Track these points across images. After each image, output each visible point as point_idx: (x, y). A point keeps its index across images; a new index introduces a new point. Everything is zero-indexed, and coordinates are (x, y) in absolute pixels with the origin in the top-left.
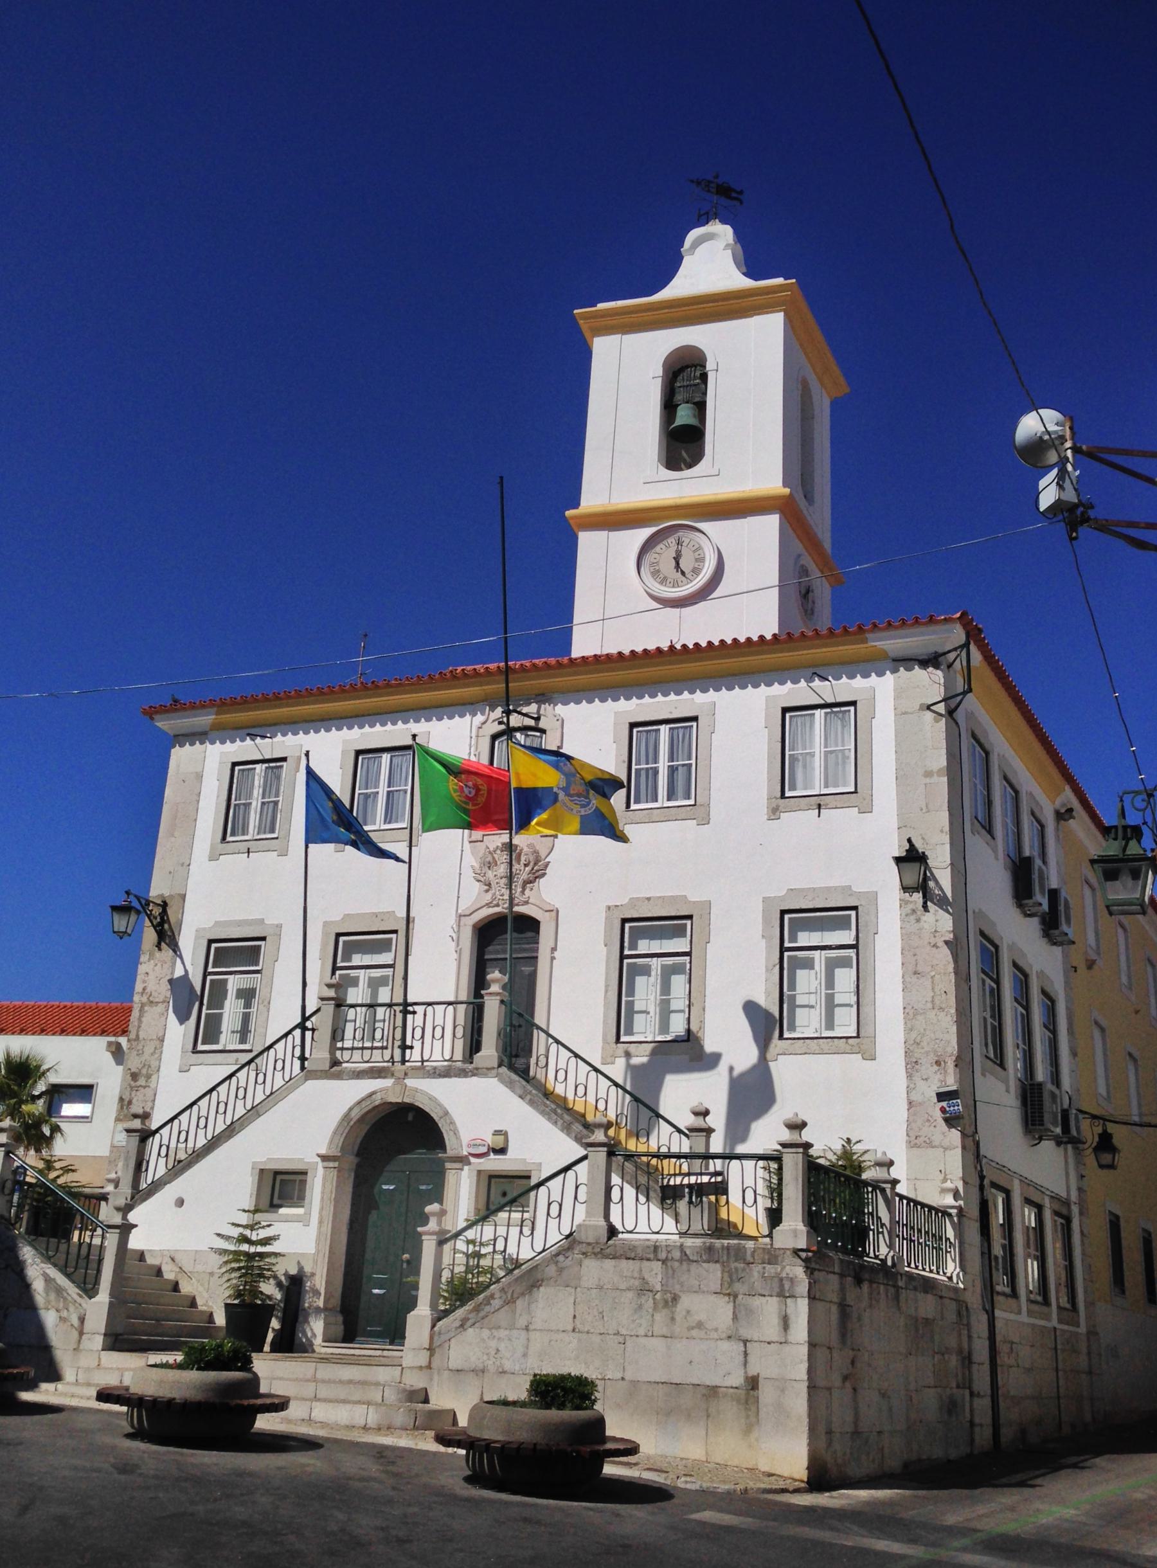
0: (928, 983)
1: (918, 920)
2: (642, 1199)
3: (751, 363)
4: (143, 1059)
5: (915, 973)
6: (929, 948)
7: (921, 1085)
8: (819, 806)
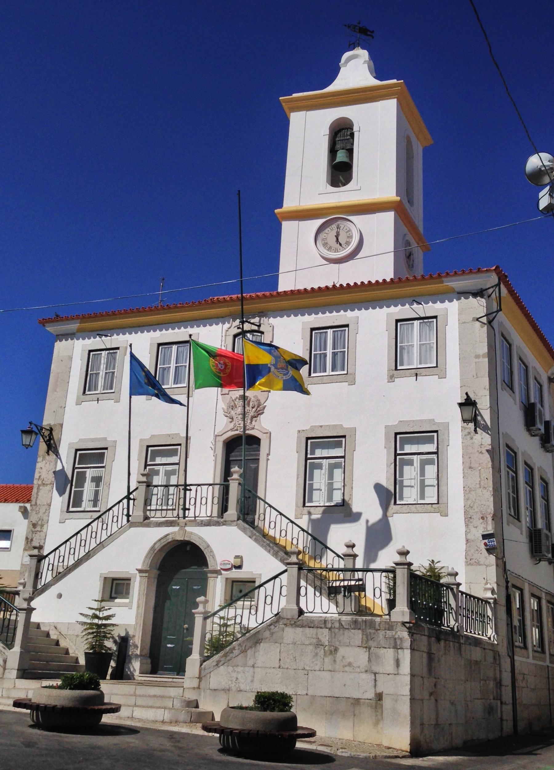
0: (477, 474)
1: (472, 438)
2: (318, 594)
3: (379, 127)
4: (39, 516)
5: (470, 468)
6: (477, 454)
7: (473, 530)
8: (416, 375)
